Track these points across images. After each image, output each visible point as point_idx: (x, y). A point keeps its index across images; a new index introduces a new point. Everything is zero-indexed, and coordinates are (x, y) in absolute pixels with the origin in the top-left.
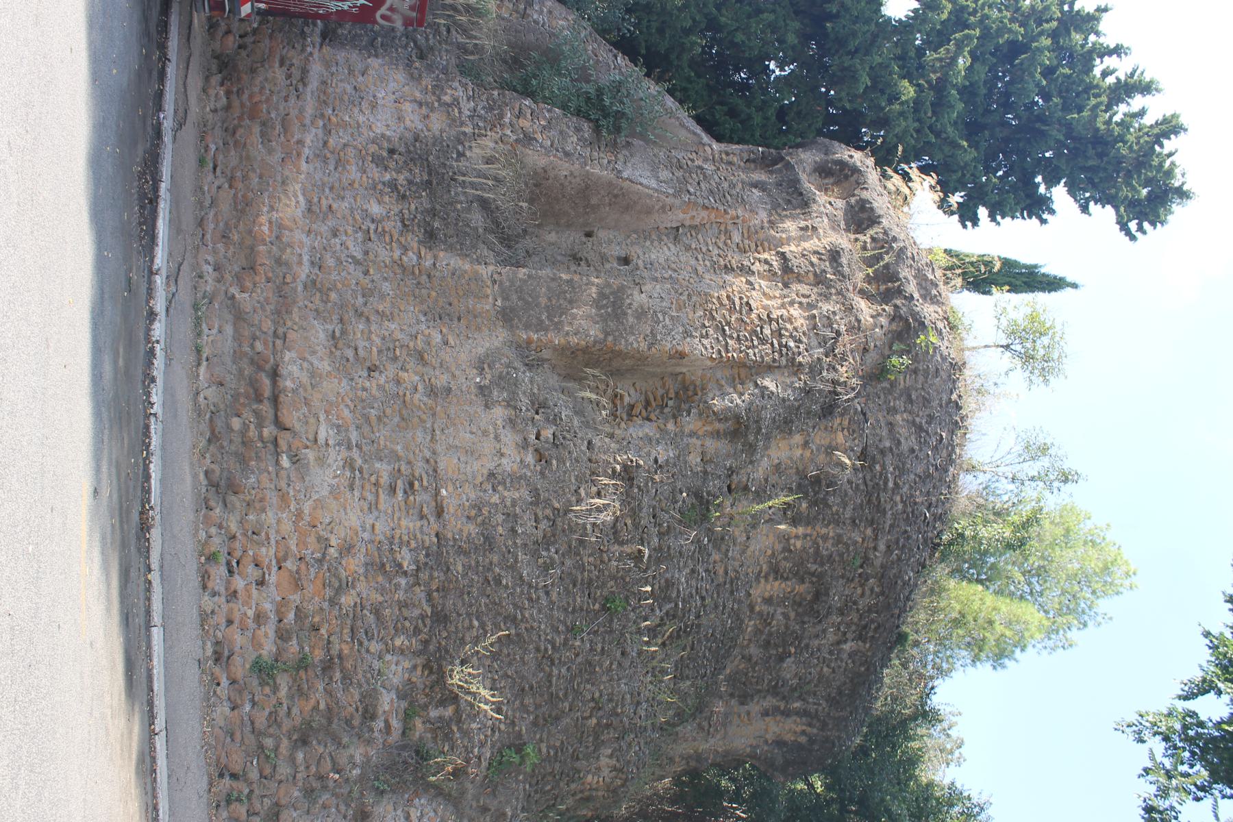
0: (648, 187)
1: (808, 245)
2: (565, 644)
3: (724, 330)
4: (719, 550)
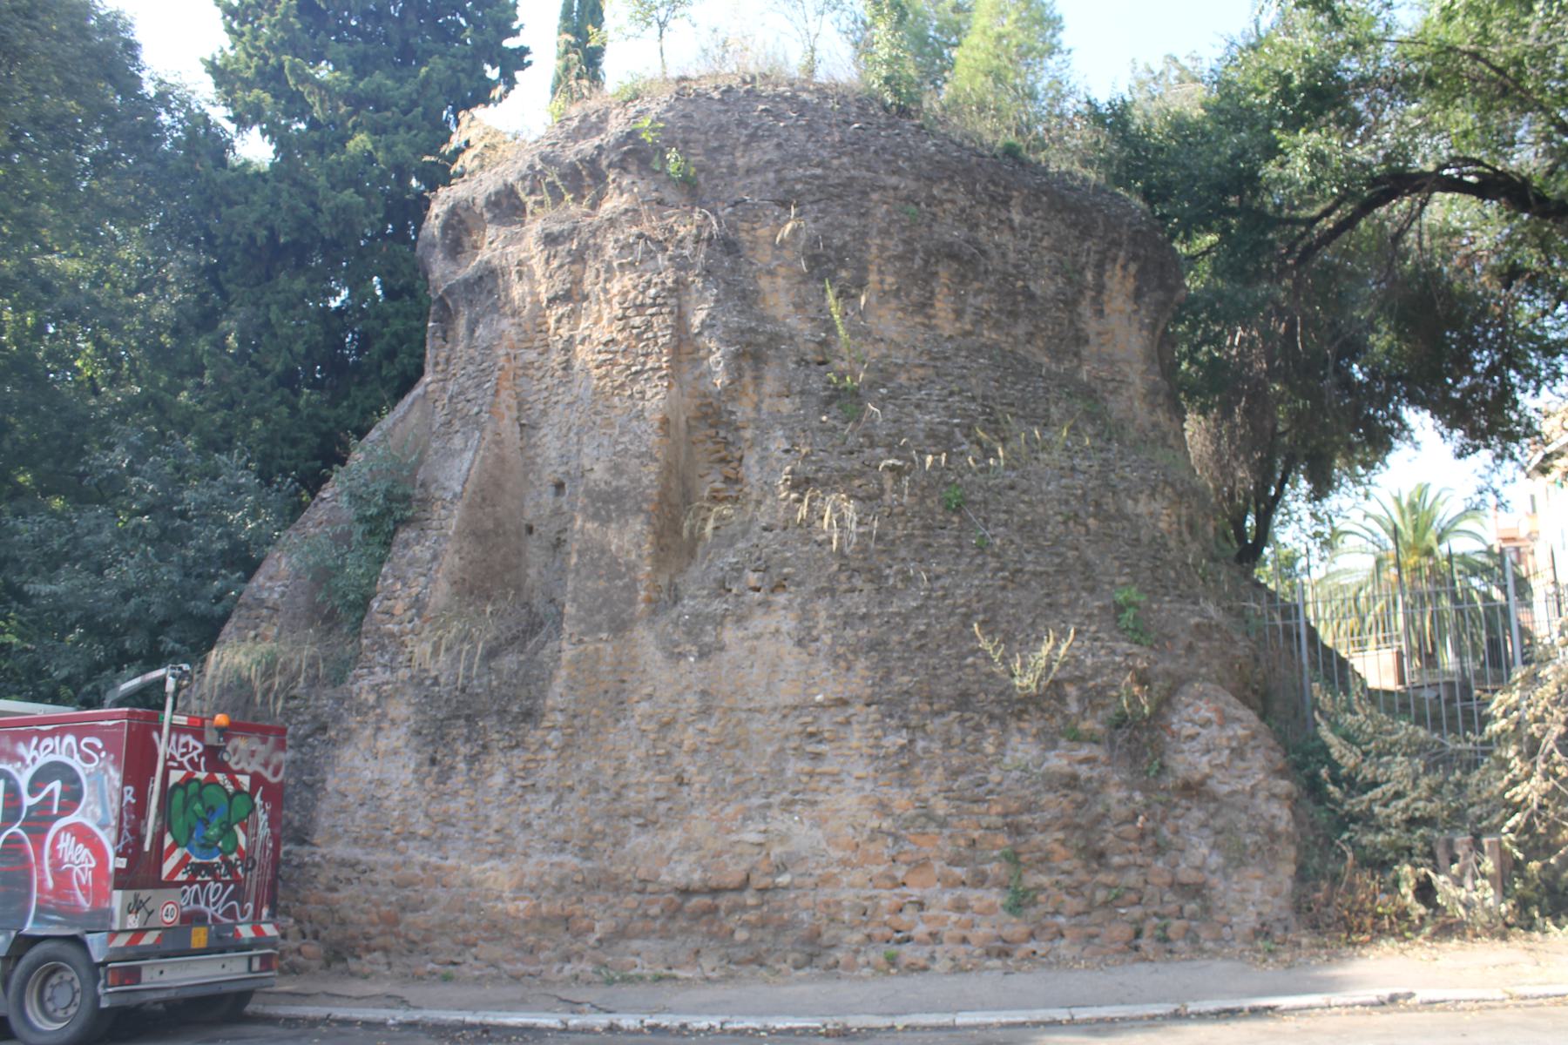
0: (473, 462)
1: (539, 272)
2: (997, 556)
4: (895, 374)
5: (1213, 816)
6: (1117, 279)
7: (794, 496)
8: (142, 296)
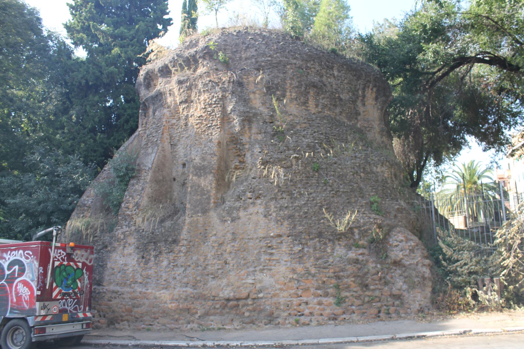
0: (155, 157)
1: (176, 93)
2: (331, 186)
3: (209, 126)
4: (296, 126)
5: (404, 272)
6: (369, 93)
7: (262, 167)
8: (44, 103)
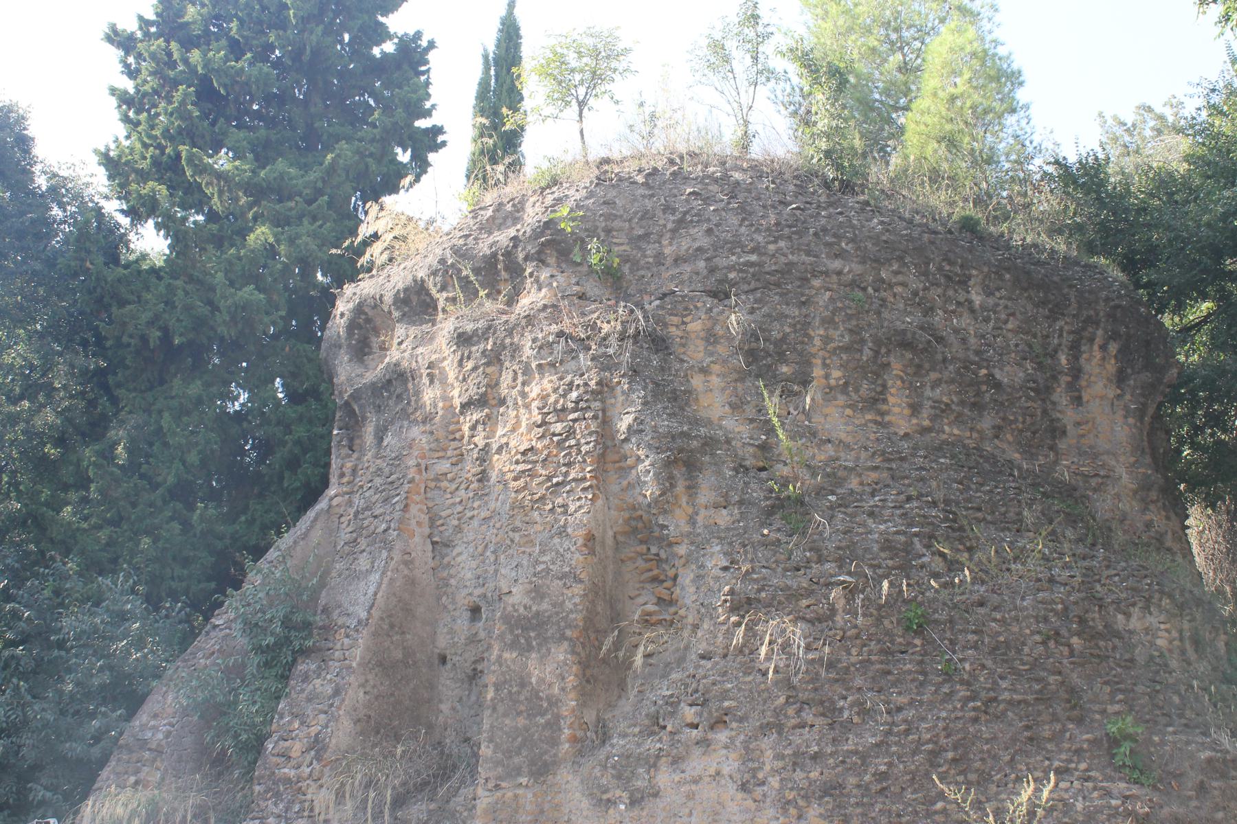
0: (380, 585)
2: (968, 684)
3: (558, 484)
4: (845, 479)
7: (734, 619)
8: (26, 404)
